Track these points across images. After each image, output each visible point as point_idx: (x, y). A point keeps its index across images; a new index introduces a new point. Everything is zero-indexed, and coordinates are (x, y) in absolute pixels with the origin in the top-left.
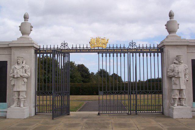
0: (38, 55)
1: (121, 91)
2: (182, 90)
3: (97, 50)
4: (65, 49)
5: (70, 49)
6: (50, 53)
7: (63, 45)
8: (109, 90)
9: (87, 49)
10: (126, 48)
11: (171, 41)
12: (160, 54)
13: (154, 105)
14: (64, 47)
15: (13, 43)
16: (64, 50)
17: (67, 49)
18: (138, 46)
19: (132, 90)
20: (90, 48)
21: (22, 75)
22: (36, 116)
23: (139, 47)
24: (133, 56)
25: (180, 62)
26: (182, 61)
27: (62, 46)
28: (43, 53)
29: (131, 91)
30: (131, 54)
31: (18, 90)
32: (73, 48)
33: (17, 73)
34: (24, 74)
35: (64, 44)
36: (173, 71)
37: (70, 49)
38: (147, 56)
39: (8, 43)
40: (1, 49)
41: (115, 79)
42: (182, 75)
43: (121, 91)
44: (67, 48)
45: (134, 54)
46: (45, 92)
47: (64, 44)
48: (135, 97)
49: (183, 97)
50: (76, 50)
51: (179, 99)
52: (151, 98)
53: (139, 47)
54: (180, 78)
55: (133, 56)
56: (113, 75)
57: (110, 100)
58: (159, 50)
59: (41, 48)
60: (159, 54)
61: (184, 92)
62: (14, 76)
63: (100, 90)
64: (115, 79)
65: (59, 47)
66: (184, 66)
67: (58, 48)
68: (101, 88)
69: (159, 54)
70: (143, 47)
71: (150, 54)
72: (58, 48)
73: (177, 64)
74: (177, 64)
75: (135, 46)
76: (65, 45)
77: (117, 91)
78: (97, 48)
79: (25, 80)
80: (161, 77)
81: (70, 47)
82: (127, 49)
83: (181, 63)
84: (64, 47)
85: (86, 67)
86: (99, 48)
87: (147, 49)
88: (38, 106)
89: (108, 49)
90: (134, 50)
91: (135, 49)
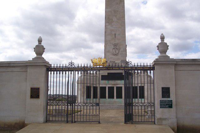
3: (108, 68)
4: (72, 67)
6: (141, 70)
9: (90, 68)
13: (92, 115)
14: (71, 66)
15: (16, 63)
16: (71, 68)
17: (73, 68)
18: (133, 65)
20: (92, 67)
22: (47, 124)
23: (134, 65)
24: (71, 74)
28: (135, 70)
32: (78, 66)
35: (71, 63)
37: (76, 68)
38: (57, 74)
39: (25, 63)
40: (1, 67)
47: (71, 63)
50: (112, 68)
52: (94, 110)
53: (134, 65)
55: (71, 74)
57: (56, 109)
60: (55, 72)
65: (67, 66)
67: (66, 66)
69: (55, 72)
70: (138, 65)
71: (150, 71)
72: (66, 66)
78: (99, 67)
81: (76, 66)
82: (124, 67)
84: (71, 66)
86: (101, 66)
87: (141, 67)
88: (48, 115)
89: (108, 67)
90: (130, 68)
91: (131, 67)
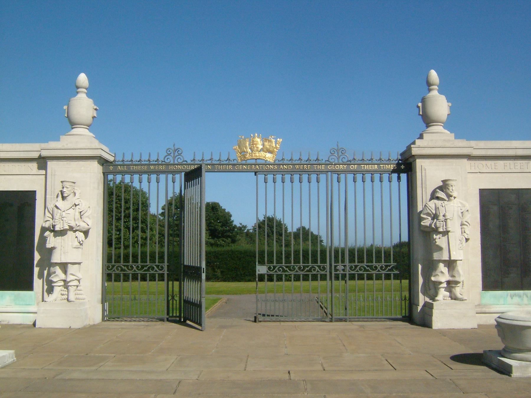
0: (110, 177)
1: (310, 264)
2: (455, 261)
4: (176, 162)
5: (189, 162)
7: (172, 155)
8: (363, 262)
10: (323, 162)
11: (431, 145)
12: (404, 176)
19: (337, 261)
21: (73, 224)
25: (451, 196)
26: (454, 194)
27: (169, 155)
29: (333, 264)
30: (335, 176)
31: (64, 261)
33: (62, 218)
34: (77, 223)
36: (435, 217)
41: (305, 239)
42: (454, 226)
43: (392, 263)
44: (180, 161)
45: (342, 176)
46: (127, 266)
48: (176, 289)
49: (457, 279)
51: (448, 282)
54: (449, 234)
56: (298, 230)
58: (403, 167)
59: (119, 161)
61: (460, 267)
62: (54, 226)
63: (259, 262)
64: (305, 239)
66: (460, 205)
68: (262, 253)
73: (443, 199)
74: (443, 199)
75: (344, 156)
76: (176, 154)
77: (383, 264)
79: (81, 236)
80: (184, 173)
83: (453, 198)
85: (221, 207)
